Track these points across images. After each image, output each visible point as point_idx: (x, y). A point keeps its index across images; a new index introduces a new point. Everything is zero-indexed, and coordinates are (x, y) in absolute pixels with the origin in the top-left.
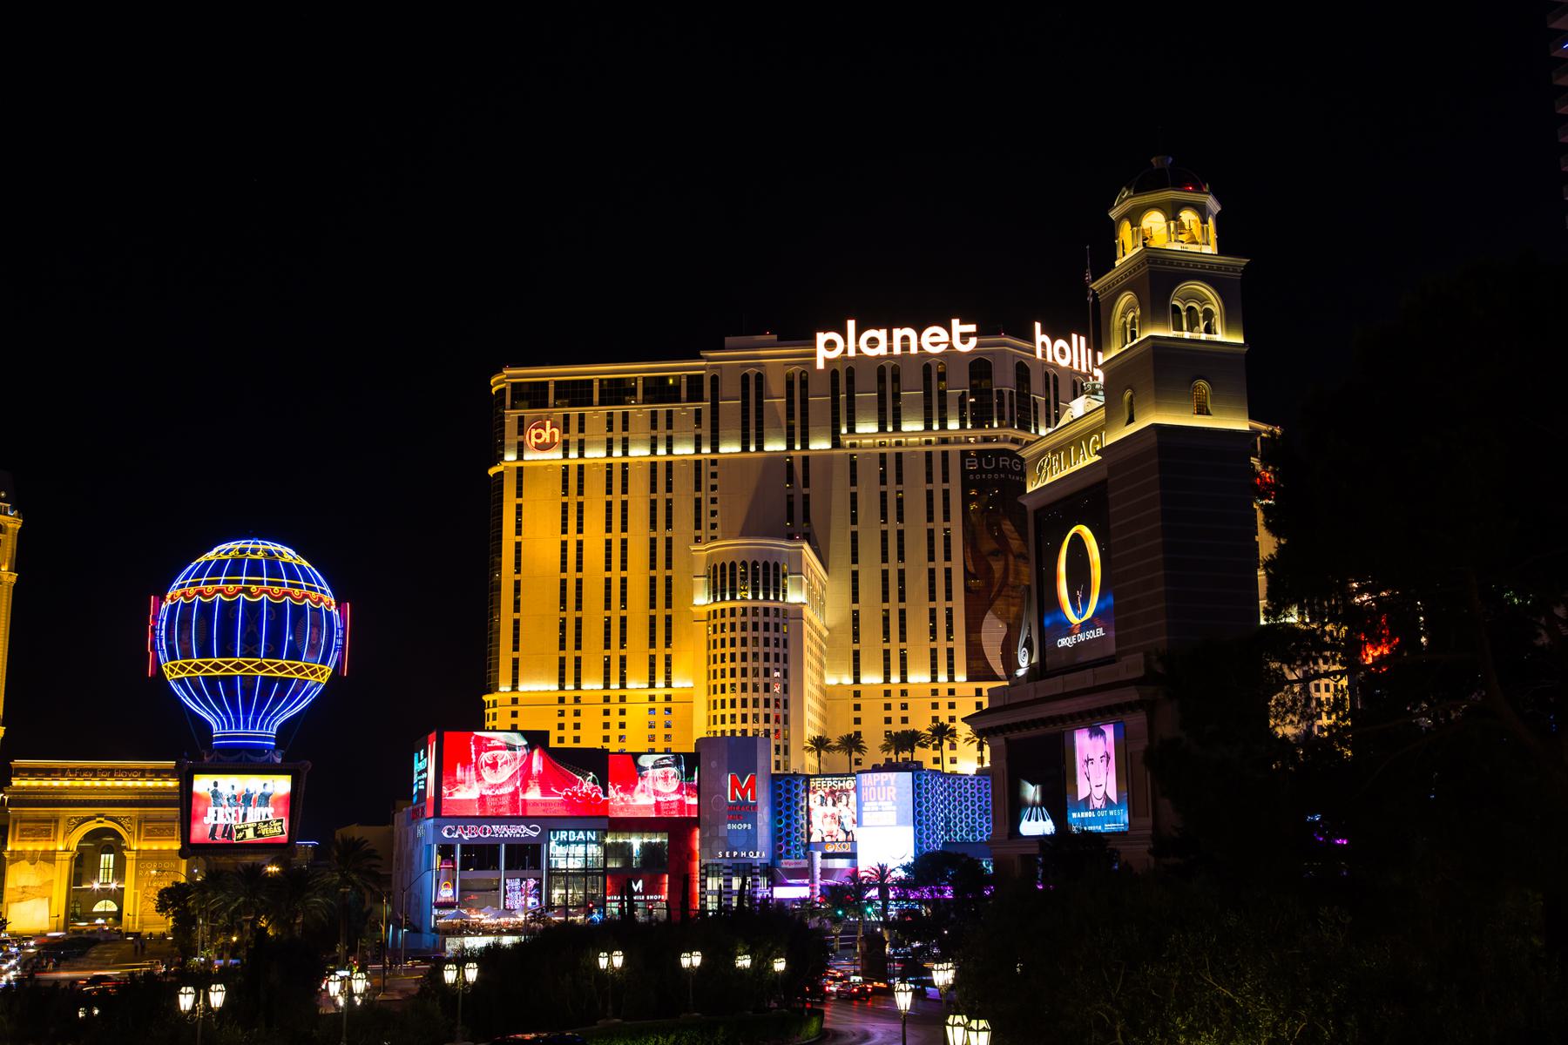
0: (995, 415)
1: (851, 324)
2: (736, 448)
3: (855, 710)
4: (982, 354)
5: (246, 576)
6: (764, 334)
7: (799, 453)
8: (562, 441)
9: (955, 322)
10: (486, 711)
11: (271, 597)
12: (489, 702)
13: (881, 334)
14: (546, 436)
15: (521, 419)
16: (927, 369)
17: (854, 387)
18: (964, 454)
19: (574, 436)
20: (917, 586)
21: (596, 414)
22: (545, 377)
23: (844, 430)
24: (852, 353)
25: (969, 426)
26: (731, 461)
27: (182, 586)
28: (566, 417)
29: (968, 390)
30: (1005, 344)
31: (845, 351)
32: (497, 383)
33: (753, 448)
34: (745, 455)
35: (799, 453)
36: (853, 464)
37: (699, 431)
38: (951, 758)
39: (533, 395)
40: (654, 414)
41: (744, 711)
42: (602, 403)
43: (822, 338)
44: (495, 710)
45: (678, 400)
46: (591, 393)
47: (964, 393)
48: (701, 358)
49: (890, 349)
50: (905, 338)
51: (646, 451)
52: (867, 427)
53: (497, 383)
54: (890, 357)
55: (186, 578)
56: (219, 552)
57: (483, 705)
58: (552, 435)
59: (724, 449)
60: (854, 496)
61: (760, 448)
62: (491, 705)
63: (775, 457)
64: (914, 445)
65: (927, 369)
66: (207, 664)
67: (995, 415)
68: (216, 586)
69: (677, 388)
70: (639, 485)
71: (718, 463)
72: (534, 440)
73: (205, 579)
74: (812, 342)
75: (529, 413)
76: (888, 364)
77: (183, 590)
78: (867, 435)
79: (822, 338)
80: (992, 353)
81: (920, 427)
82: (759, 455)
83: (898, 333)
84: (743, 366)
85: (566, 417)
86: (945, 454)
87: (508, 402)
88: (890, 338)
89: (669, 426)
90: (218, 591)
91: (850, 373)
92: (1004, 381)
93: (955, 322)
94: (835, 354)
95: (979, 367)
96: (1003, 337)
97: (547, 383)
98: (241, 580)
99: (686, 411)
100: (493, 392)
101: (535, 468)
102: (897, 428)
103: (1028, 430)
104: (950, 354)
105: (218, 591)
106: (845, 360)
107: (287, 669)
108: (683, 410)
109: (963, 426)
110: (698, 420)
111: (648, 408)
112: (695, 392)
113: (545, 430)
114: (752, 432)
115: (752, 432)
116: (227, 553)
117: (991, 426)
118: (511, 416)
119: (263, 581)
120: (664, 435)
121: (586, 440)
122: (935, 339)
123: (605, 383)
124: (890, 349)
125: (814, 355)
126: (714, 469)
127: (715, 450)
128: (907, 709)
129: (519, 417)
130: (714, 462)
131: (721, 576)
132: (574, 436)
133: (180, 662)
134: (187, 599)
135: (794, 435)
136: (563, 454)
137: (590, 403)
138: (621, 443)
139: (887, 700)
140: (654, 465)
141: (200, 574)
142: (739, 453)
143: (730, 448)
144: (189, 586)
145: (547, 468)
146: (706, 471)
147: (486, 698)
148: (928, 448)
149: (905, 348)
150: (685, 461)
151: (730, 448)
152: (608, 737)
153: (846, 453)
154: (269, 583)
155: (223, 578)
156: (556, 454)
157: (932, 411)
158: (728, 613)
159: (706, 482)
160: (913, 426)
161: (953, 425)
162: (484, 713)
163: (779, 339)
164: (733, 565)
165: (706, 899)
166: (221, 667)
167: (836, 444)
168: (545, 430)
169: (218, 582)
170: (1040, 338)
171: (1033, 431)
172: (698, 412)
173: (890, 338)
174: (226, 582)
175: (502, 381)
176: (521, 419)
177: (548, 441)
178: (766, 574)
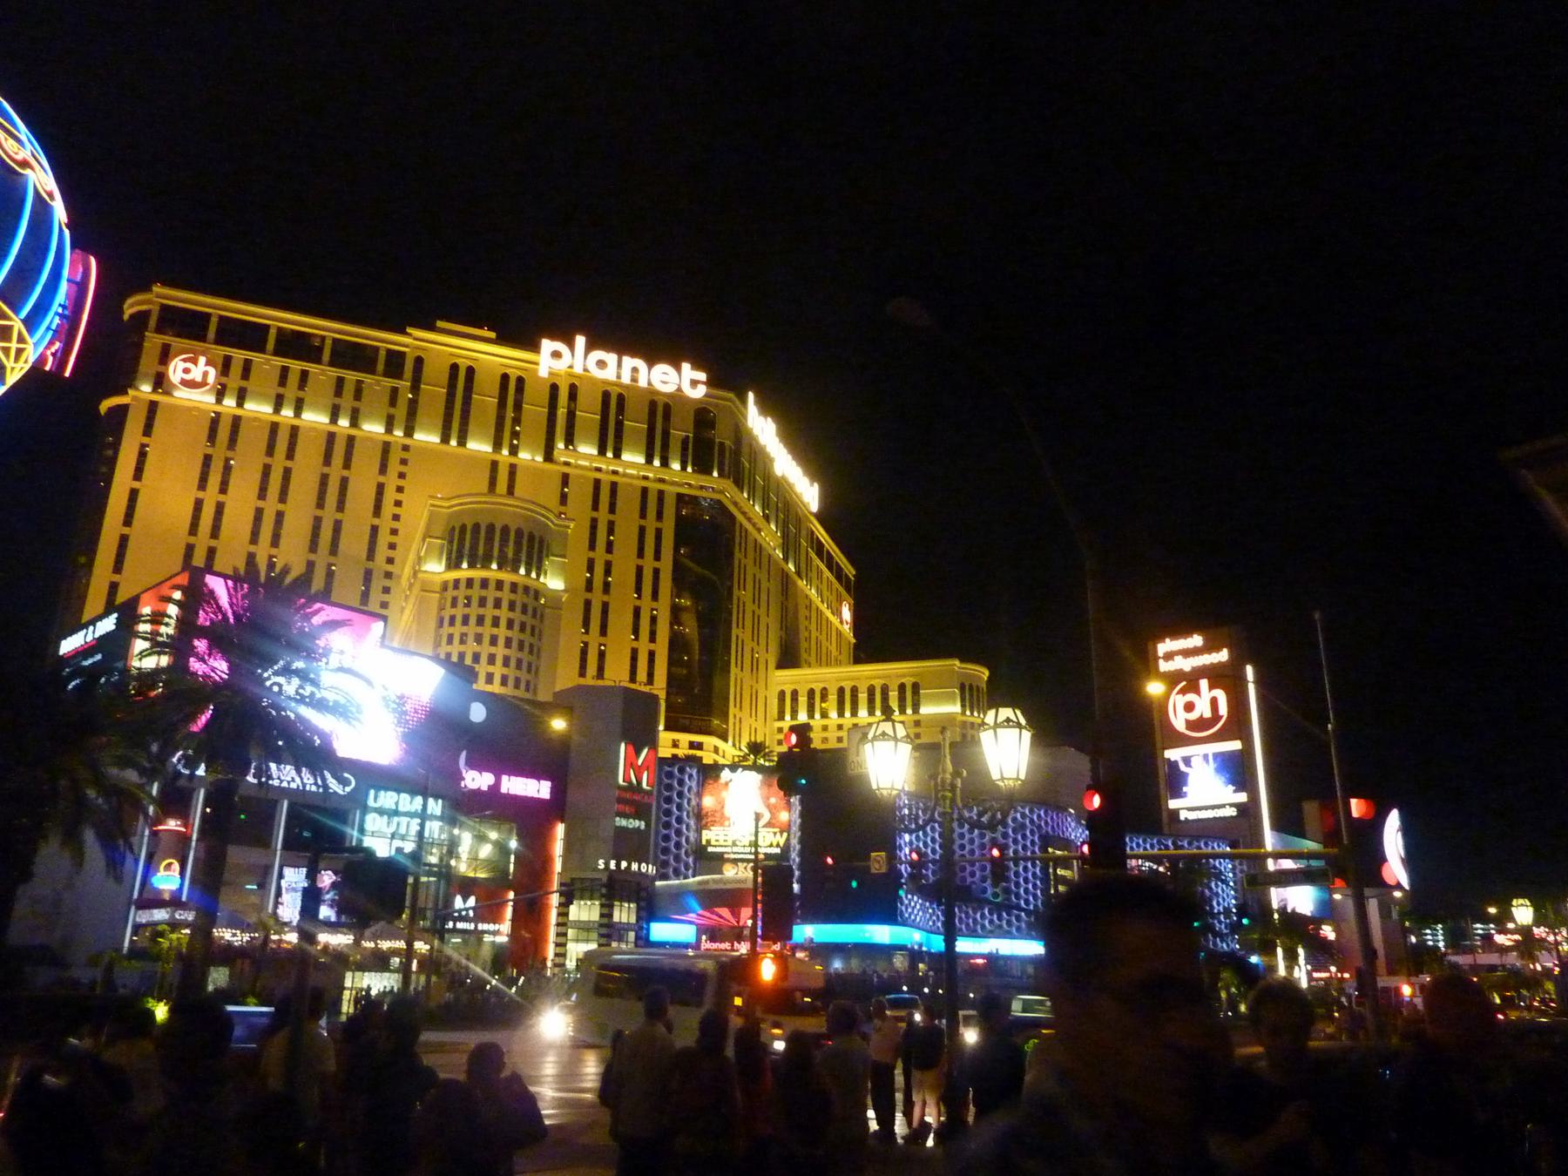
0: (716, 461)
1: (580, 341)
7: (505, 458)
13: (611, 358)
14: (196, 373)
16: (653, 405)
17: (522, 398)
18: (680, 497)
19: (234, 381)
20: (620, 621)
21: (267, 363)
22: (196, 305)
23: (561, 445)
24: (578, 369)
25: (689, 469)
26: (426, 450)
29: (691, 435)
32: (132, 306)
34: (444, 447)
35: (505, 458)
36: (565, 479)
39: (190, 326)
40: (285, 371)
42: (276, 353)
43: (548, 345)
45: (318, 361)
46: (265, 341)
49: (619, 377)
50: (635, 370)
53: (132, 306)
59: (419, 436)
61: (462, 442)
64: (631, 476)
65: (653, 405)
67: (716, 461)
69: (320, 349)
71: (411, 449)
75: (176, 342)
76: (615, 391)
78: (633, 465)
79: (548, 345)
80: (717, 406)
81: (641, 460)
82: (461, 450)
86: (661, 493)
91: (621, 398)
92: (722, 435)
93: (686, 366)
94: (561, 366)
95: (703, 417)
97: (208, 316)
99: (326, 375)
102: (617, 455)
104: (678, 395)
106: (569, 375)
108: (378, 384)
109: (684, 468)
110: (393, 402)
114: (455, 425)
115: (455, 425)
118: (153, 341)
120: (153, 371)
121: (249, 389)
122: (665, 378)
124: (619, 377)
126: (405, 455)
130: (406, 448)
132: (234, 381)
137: (262, 350)
140: (331, 437)
142: (270, 414)
143: (427, 437)
145: (190, 411)
148: (645, 483)
149: (634, 380)
150: (315, 429)
151: (427, 437)
156: (205, 398)
157: (656, 446)
159: (394, 467)
160: (633, 457)
161: (676, 466)
165: (565, 935)
167: (549, 457)
172: (394, 392)
177: (1208, 714)
178: (531, 547)
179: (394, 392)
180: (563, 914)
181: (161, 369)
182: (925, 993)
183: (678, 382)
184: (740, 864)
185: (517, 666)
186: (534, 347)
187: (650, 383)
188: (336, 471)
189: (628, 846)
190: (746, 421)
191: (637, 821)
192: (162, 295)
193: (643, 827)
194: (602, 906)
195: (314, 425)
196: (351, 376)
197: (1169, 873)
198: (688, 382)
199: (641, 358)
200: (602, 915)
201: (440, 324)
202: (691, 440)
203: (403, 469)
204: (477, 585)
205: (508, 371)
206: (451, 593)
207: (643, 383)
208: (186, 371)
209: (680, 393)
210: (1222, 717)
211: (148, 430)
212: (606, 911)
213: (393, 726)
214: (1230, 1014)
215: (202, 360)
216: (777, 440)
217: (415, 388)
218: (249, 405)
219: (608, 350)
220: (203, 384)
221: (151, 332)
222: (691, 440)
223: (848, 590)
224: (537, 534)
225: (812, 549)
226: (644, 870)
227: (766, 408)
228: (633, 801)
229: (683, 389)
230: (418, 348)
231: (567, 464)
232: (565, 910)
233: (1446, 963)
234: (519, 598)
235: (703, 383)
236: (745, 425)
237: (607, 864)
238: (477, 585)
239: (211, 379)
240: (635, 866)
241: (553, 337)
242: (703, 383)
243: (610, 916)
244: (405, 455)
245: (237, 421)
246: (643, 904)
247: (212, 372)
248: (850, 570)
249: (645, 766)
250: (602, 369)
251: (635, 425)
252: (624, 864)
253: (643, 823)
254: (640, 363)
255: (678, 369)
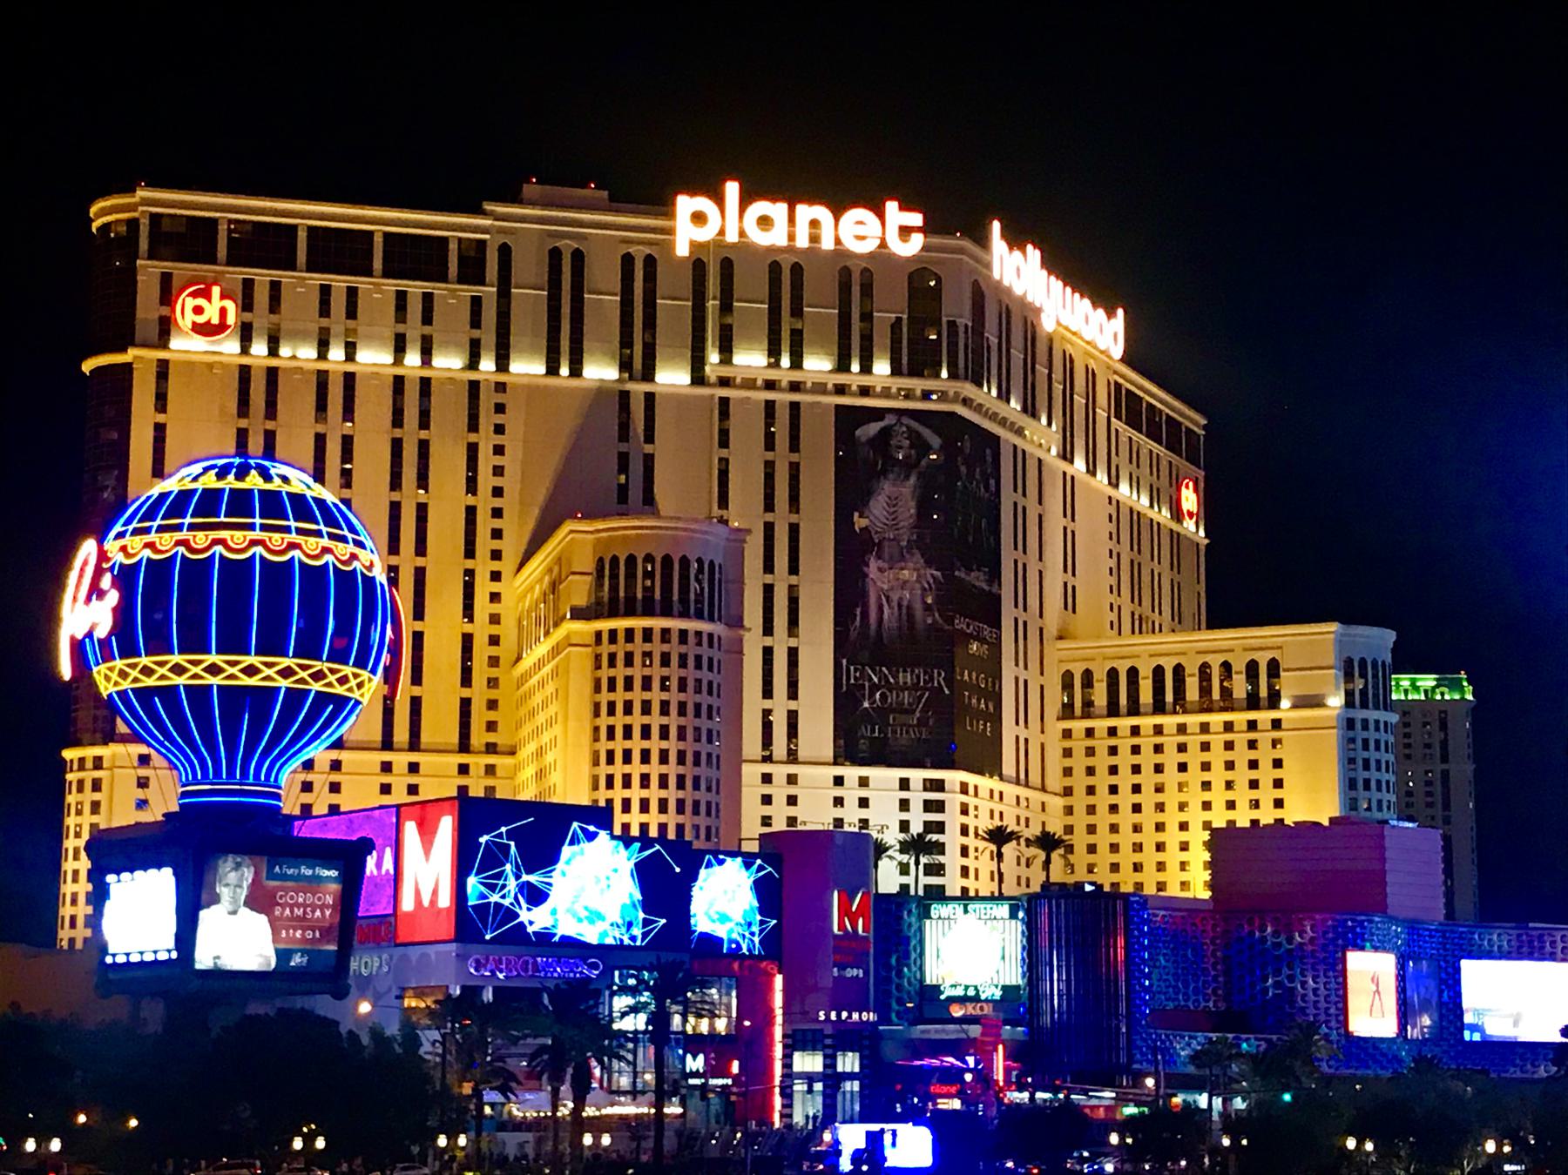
0: (944, 358)
1: (732, 189)
2: (539, 368)
3: (789, 804)
4: (927, 263)
5: (225, 516)
6: (585, 186)
8: (239, 324)
9: (892, 207)
10: (69, 777)
11: (308, 556)
12: (72, 761)
13: (779, 210)
14: (211, 314)
15: (166, 279)
16: (845, 275)
19: (261, 318)
21: (301, 284)
24: (732, 237)
27: (121, 535)
28: (248, 285)
29: (905, 317)
30: (962, 251)
31: (722, 232)
32: (104, 212)
33: (564, 371)
37: (476, 333)
38: (1117, 812)
41: (645, 793)
42: (311, 268)
43: (685, 204)
44: (97, 774)
47: (899, 320)
48: (484, 213)
49: (791, 237)
50: (814, 224)
51: (387, 357)
52: (751, 359)
53: (104, 212)
54: (791, 249)
55: (127, 523)
56: (183, 478)
57: (62, 766)
58: (223, 312)
60: (724, 462)
61: (576, 372)
62: (75, 766)
63: (601, 392)
65: (845, 275)
66: (161, 664)
67: (944, 358)
68: (178, 536)
70: (373, 410)
72: (190, 317)
73: (158, 522)
74: (667, 209)
75: (181, 270)
76: (786, 262)
77: (121, 542)
79: (685, 204)
82: (575, 382)
83: (805, 212)
84: (551, 234)
85: (248, 285)
87: (144, 245)
88: (792, 220)
89: (427, 319)
90: (254, 543)
92: (957, 309)
93: (892, 207)
94: (706, 234)
96: (958, 238)
98: (183, 524)
100: (94, 230)
101: (190, 365)
103: (980, 386)
105: (254, 543)
106: (719, 246)
107: (295, 673)
108: (452, 296)
111: (392, 285)
112: (472, 270)
113: (209, 300)
116: (195, 479)
117: (937, 375)
118: (148, 271)
119: (254, 524)
122: (861, 231)
123: (165, 222)
124: (791, 237)
125: (671, 231)
126: (500, 398)
127: (502, 364)
128: (1071, 795)
129: (163, 274)
131: (617, 576)
132: (261, 318)
133: (145, 660)
134: (128, 555)
135: (559, 353)
136: (269, 348)
137: (292, 266)
138: (419, 344)
139: (838, 792)
141: (150, 515)
143: (527, 367)
144: (157, 532)
145: (207, 368)
146: (487, 400)
147: (69, 754)
149: (815, 239)
151: (527, 367)
152: (1140, 805)
153: (712, 396)
154: (264, 528)
155: (188, 520)
156: (229, 346)
158: (621, 637)
159: (487, 419)
160: (818, 364)
161: (882, 367)
162: (65, 780)
163: (612, 198)
164: (631, 560)
166: (221, 670)
167: (698, 379)
168: (209, 300)
169: (179, 528)
170: (998, 244)
171: (985, 389)
172: (476, 302)
173: (792, 220)
174: (192, 527)
175: (104, 212)
176: (166, 279)
177: (215, 321)
179: (476, 302)
180: (787, 1065)
181: (165, 311)
182: (127, 1121)
183: (880, 235)
184: (968, 1004)
185: (707, 764)
186: (665, 207)
187: (838, 241)
188: (411, 433)
189: (846, 995)
190: (992, 272)
191: (855, 970)
192: (148, 200)
193: (861, 975)
194: (825, 1057)
195: (375, 369)
196: (415, 288)
197: (928, 1115)
198: (896, 231)
199: (820, 203)
200: (825, 1066)
201: (531, 189)
202: (905, 322)
203: (499, 419)
204: (638, 637)
205: (632, 250)
206: (606, 649)
207: (827, 244)
208: (198, 310)
209: (883, 250)
210: (230, 326)
211: (161, 402)
212: (828, 1062)
213: (628, 901)
214: (743, 1079)
215: (216, 291)
216: (1045, 273)
217: (504, 294)
218: (285, 351)
219: (774, 199)
220: (221, 327)
221: (143, 259)
222: (905, 322)
223: (1192, 459)
224: (692, 558)
225: (1118, 417)
226: (865, 1019)
227: (1015, 240)
228: (849, 948)
229: (889, 245)
230: (501, 231)
231: (724, 382)
232: (788, 1061)
233: (827, 1137)
234: (691, 650)
235: (918, 230)
236: (990, 277)
237: (827, 1016)
238: (638, 637)
239: (231, 319)
240: (855, 1016)
241: (693, 192)
242: (918, 230)
243: (834, 1066)
244: (500, 398)
245: (272, 373)
246: (866, 1052)
247: (230, 306)
248: (1194, 420)
249: (861, 910)
250: (767, 230)
251: (821, 312)
252: (844, 1015)
253: (861, 971)
254: (822, 213)
255: (881, 215)
